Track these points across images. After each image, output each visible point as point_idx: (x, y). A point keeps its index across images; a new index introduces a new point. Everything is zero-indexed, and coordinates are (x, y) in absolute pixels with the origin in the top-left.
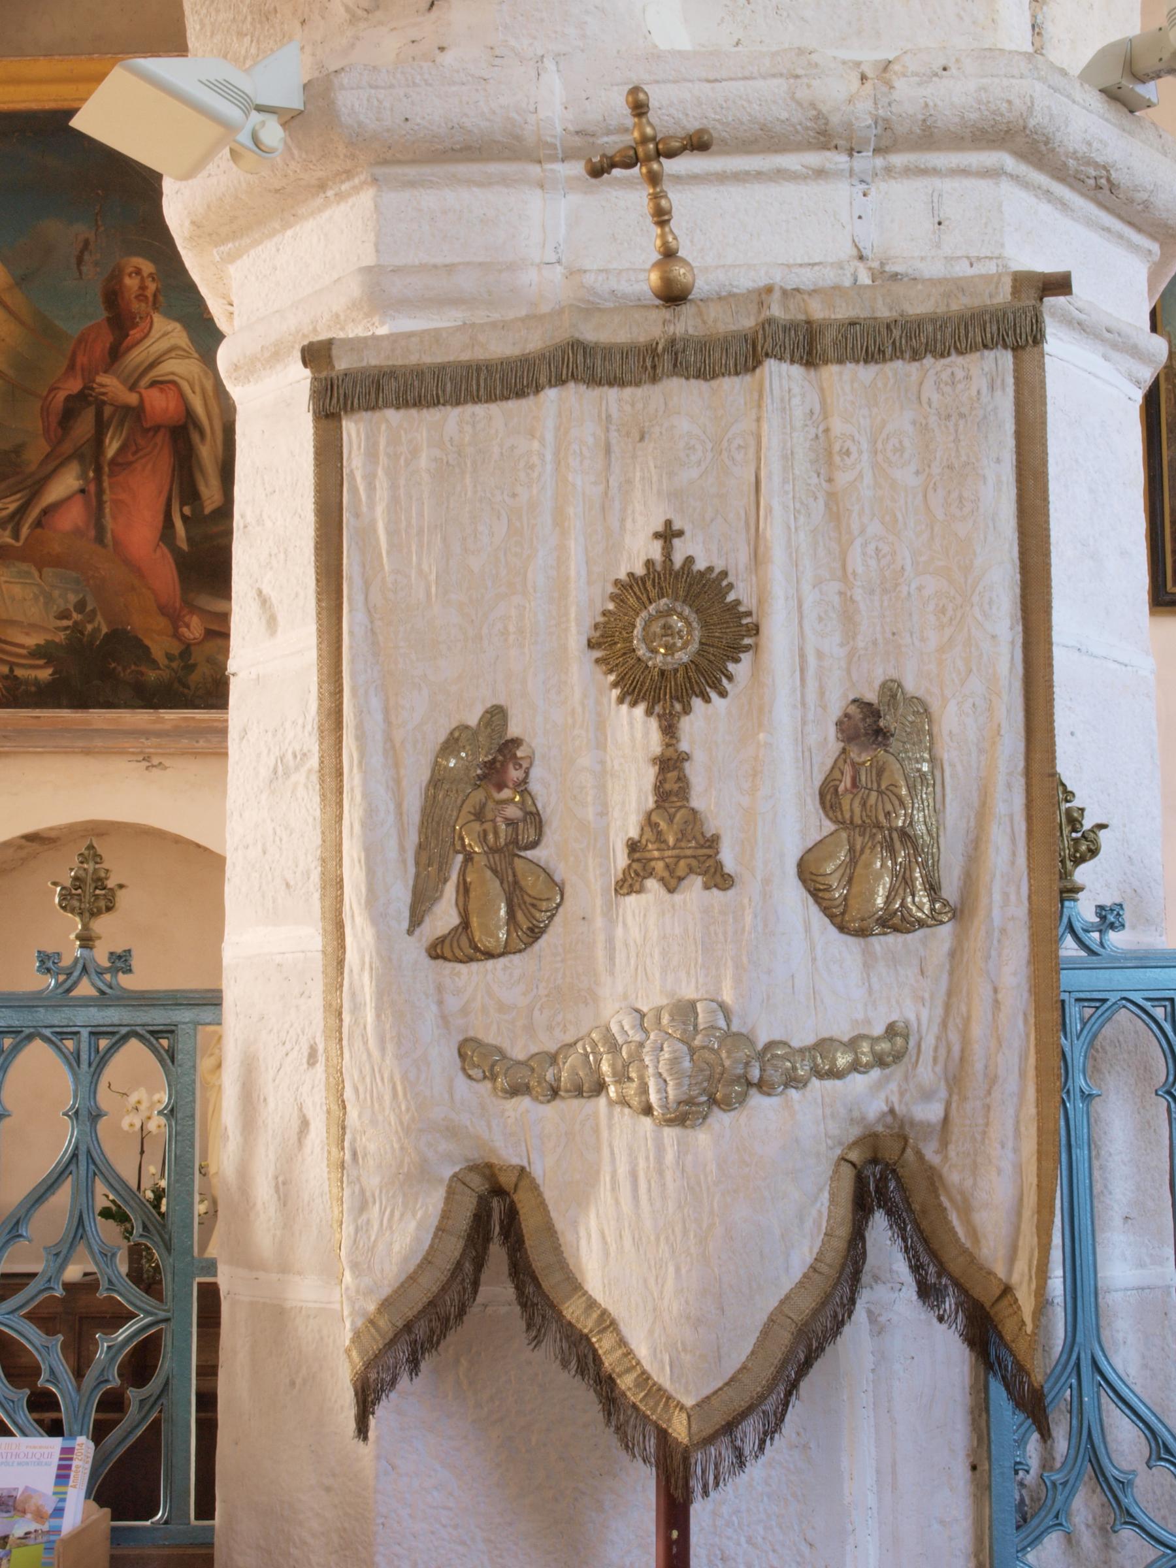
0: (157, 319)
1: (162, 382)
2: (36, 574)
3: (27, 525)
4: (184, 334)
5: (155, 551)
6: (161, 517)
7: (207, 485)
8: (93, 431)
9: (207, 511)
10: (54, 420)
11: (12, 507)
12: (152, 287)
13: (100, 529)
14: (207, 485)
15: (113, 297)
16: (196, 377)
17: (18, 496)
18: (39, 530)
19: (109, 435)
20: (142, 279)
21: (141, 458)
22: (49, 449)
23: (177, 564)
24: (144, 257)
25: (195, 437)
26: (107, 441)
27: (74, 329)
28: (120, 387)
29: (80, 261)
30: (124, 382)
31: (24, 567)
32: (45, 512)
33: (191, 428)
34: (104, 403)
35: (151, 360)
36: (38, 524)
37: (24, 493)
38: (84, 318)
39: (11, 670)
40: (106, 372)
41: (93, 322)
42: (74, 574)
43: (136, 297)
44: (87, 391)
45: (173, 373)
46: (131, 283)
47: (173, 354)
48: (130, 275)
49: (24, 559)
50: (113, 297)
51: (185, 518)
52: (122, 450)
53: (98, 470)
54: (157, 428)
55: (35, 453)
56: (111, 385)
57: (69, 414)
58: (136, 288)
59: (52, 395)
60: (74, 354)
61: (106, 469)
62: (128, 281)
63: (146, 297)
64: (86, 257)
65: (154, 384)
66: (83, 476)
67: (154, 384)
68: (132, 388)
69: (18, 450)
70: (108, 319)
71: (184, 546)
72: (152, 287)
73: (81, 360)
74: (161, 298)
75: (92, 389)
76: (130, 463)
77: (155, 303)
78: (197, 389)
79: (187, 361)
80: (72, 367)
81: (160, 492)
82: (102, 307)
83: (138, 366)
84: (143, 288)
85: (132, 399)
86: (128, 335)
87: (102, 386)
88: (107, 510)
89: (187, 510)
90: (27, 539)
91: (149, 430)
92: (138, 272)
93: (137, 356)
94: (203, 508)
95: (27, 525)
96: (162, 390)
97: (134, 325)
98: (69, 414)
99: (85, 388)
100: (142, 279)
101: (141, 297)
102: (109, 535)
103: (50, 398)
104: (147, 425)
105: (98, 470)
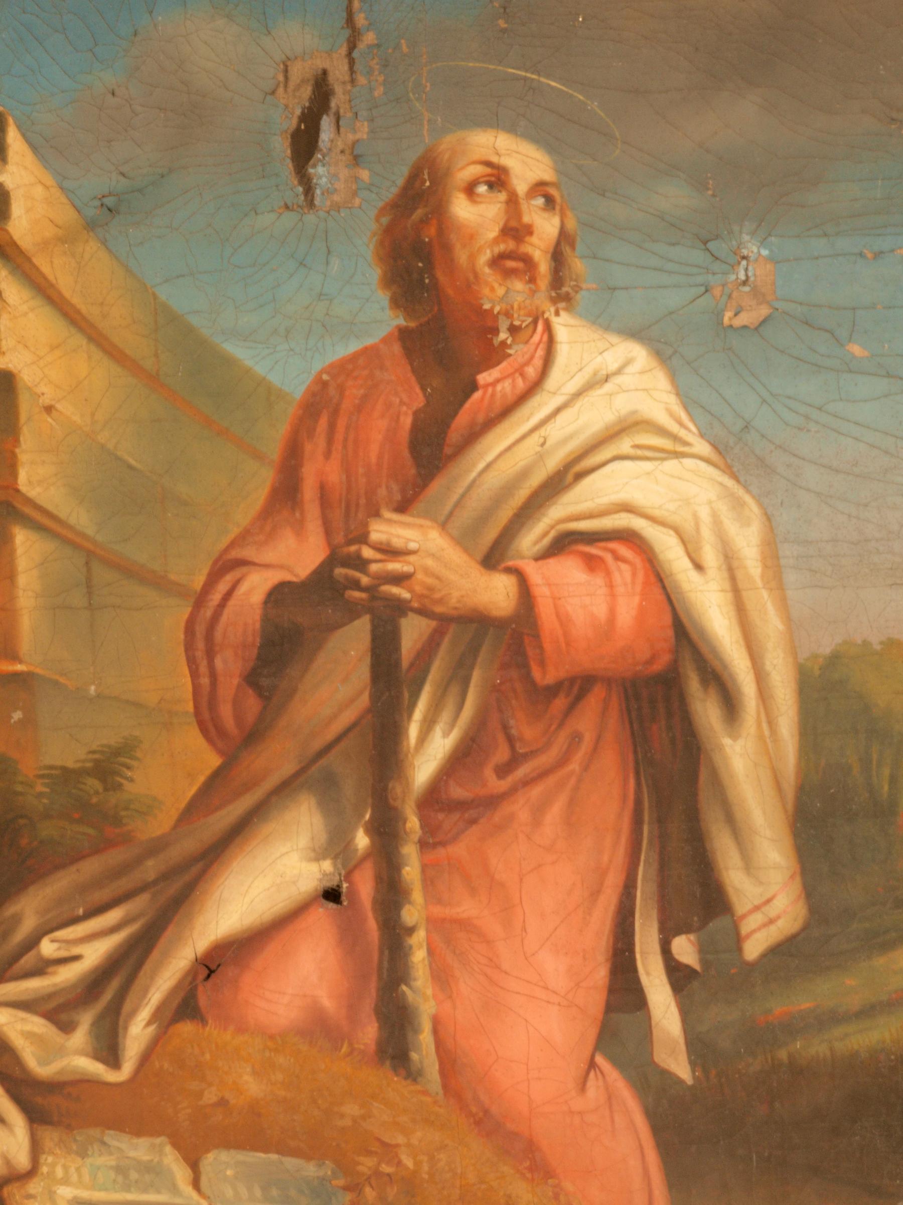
0: (566, 327)
1: (593, 538)
2: (181, 1173)
3: (145, 1014)
4: (660, 381)
5: (582, 1087)
6: (601, 974)
7: (749, 865)
8: (364, 700)
9: (753, 948)
10: (230, 666)
11: (94, 954)
12: (546, 227)
13: (396, 1021)
14: (749, 865)
15: (415, 256)
16: (704, 514)
17: (113, 916)
18: (187, 1028)
19: (418, 714)
20: (513, 201)
21: (527, 783)
22: (214, 761)
23: (657, 1129)
24: (512, 129)
25: (707, 711)
26: (413, 731)
27: (289, 371)
28: (455, 555)
29: (304, 145)
30: (464, 540)
31: (140, 1149)
32: (212, 966)
33: (693, 684)
34: (400, 608)
35: (552, 464)
36: (185, 1007)
37: (140, 903)
38: (310, 318)
39: (406, 543)
40: (402, 508)
41: (354, 347)
42: (311, 1170)
43: (497, 261)
44: (339, 572)
45: (627, 508)
46: (475, 216)
47: (625, 445)
48: (470, 190)
49: (137, 1124)
50: (415, 256)
51: (679, 976)
52: (462, 759)
53: (386, 830)
54: (580, 685)
55: (170, 772)
56: (422, 547)
57: (281, 649)
58: (492, 233)
59: (222, 587)
60: (293, 457)
61: (413, 823)
62: (462, 209)
63: (528, 261)
64: (326, 133)
65: (563, 543)
66: (336, 845)
67: (563, 543)
68: (493, 559)
69: (108, 767)
70: (404, 334)
71: (681, 1069)
72: (546, 227)
73: (319, 469)
74: (578, 264)
75: (361, 564)
76: (493, 802)
77: (557, 281)
78: (710, 556)
79: (672, 465)
80: (286, 492)
81: (595, 894)
82: (383, 298)
83: (508, 489)
84: (515, 230)
85: (496, 593)
86: (474, 387)
87: (390, 552)
88: (419, 956)
89: (685, 949)
90: (145, 1058)
91: (553, 691)
92: (498, 179)
93: (503, 457)
94: (738, 941)
95: (145, 1014)
96: (592, 563)
97: (493, 355)
98: (281, 649)
99: (333, 560)
100: (513, 201)
101: (512, 261)
102: (426, 1037)
103: (216, 597)
104: (545, 677)
105: (386, 830)
